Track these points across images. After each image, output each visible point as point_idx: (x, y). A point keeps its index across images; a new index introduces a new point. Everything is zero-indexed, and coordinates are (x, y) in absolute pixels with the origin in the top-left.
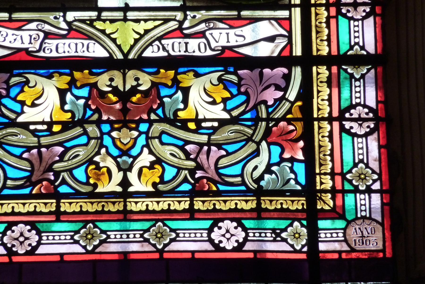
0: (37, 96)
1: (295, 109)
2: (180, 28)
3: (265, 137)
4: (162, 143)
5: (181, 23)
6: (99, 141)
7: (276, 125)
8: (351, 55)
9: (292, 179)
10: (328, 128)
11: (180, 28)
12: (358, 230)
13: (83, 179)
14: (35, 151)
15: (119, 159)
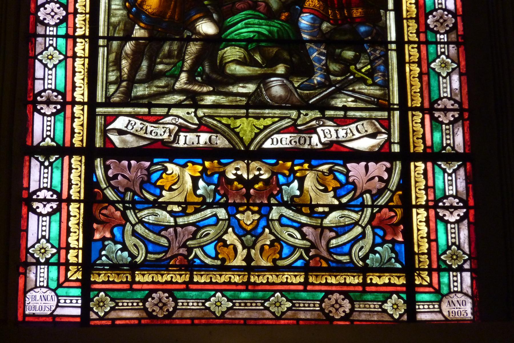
4: (282, 225)
5: (296, 120)
8: (43, 147)
9: (393, 258)
10: (425, 214)
12: (42, 297)
14: (171, 230)
15: (243, 238)
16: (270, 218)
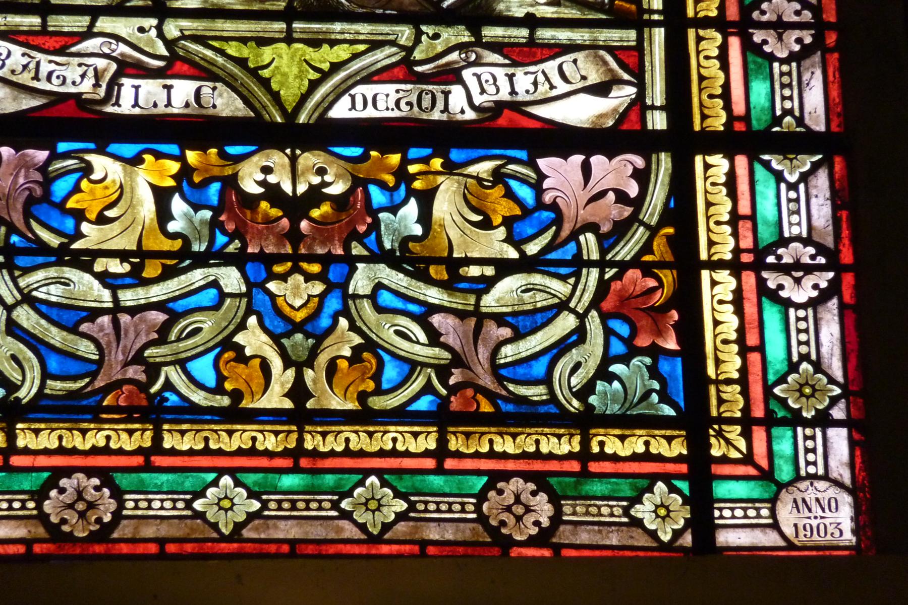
0: (105, 202)
1: (659, 244)
2: (407, 62)
3: (595, 303)
4: (380, 310)
5: (409, 50)
6: (245, 301)
7: (618, 277)
10: (732, 283)
11: (407, 62)
13: (210, 380)
14: (105, 320)
16: (351, 292)
